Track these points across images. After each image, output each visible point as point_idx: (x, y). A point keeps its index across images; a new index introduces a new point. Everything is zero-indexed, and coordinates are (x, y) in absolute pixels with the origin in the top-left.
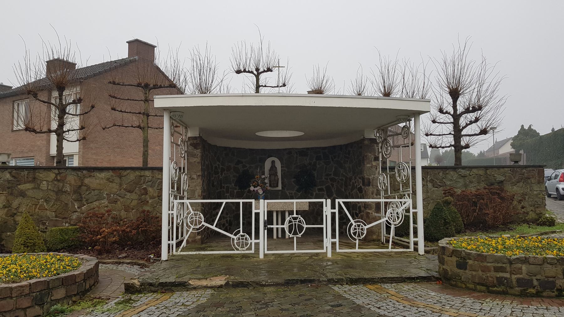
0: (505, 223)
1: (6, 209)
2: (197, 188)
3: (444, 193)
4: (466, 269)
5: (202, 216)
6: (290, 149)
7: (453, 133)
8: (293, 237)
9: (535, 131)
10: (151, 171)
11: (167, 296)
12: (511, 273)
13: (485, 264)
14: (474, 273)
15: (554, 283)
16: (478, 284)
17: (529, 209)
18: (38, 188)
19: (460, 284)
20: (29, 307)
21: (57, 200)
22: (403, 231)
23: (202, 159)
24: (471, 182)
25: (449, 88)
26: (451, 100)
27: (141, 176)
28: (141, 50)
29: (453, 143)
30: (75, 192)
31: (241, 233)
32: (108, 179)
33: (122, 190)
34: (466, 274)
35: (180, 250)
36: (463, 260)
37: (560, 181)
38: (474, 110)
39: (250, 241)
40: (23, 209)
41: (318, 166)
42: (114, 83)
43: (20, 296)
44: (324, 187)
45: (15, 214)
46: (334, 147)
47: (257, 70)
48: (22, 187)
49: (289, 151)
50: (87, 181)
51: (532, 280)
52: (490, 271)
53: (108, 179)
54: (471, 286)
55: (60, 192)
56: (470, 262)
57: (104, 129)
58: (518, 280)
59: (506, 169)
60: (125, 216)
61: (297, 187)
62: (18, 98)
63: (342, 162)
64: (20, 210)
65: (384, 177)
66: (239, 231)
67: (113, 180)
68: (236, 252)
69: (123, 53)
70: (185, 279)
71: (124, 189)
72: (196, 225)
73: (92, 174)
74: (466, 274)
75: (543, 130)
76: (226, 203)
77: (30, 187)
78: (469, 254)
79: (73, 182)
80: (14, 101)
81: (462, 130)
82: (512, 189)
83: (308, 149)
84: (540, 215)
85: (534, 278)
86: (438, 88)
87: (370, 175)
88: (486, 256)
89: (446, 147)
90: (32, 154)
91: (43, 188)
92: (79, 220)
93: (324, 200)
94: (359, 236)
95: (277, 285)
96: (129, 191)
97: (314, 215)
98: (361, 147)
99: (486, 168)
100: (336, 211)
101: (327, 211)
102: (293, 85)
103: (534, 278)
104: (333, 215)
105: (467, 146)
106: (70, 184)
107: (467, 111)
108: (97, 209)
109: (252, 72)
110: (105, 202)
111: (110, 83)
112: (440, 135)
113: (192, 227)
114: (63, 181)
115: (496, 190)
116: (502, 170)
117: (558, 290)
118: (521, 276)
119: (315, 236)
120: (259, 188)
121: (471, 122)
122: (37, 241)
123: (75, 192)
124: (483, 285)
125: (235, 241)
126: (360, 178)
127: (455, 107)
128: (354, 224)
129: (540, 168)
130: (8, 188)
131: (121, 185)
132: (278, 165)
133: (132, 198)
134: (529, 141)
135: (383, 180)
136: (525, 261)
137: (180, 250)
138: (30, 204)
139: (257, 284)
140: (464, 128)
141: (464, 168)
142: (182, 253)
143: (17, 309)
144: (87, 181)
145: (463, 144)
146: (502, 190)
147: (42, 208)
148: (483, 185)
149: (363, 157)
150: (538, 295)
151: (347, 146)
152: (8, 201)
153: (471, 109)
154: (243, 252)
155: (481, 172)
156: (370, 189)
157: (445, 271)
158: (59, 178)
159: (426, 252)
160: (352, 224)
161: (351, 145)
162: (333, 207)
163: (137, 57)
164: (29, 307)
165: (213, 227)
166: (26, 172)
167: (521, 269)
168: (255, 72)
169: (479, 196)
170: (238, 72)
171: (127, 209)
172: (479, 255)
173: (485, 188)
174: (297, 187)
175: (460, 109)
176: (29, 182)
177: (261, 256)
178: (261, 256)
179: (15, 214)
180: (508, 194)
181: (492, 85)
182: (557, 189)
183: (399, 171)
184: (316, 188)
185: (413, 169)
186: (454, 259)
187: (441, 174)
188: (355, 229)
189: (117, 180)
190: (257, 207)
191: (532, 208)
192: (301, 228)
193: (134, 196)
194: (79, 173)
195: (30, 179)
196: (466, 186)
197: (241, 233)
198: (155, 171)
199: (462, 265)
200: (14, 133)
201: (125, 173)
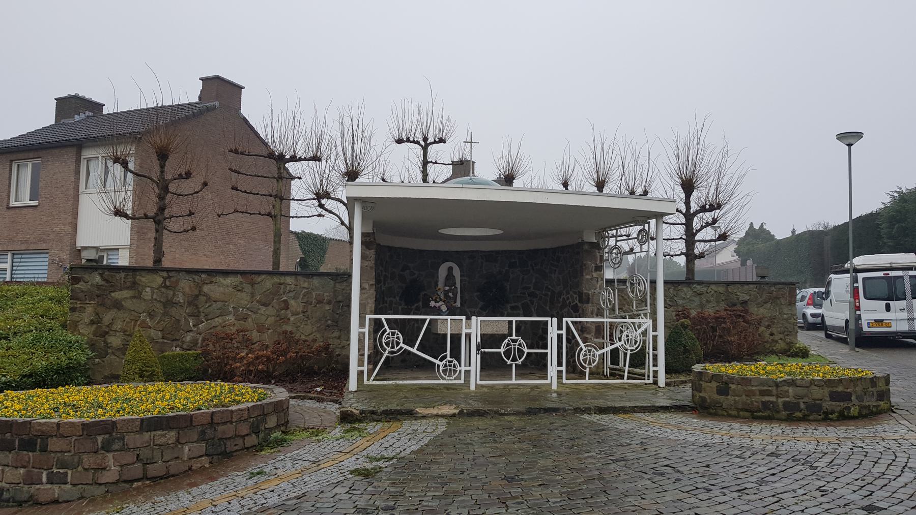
0: (751, 354)
1: (95, 326)
2: (369, 301)
3: (677, 315)
4: (728, 395)
5: (400, 335)
6: (473, 251)
7: (684, 237)
8: (511, 365)
9: (769, 233)
10: (293, 277)
11: (395, 424)
12: (778, 397)
13: (750, 388)
14: (737, 398)
15: (820, 406)
16: (742, 410)
17: (777, 337)
18: (138, 296)
19: (720, 412)
20: (247, 435)
21: (165, 314)
22: (638, 359)
23: (376, 264)
24: (708, 302)
25: (681, 178)
26: (683, 196)
27: (280, 284)
28: (221, 92)
29: (684, 251)
30: (190, 304)
31: (449, 358)
32: (235, 287)
33: (255, 302)
34: (727, 401)
35: (372, 378)
36: (724, 385)
37: (808, 304)
38: (712, 208)
39: (458, 369)
40: (118, 326)
41: (511, 276)
42: (236, 152)
43: (239, 421)
44: (519, 304)
45: (107, 333)
46: (536, 251)
47: (425, 139)
48: (116, 295)
49: (472, 255)
50: (206, 289)
51: (799, 403)
52: (754, 395)
53: (235, 287)
54: (734, 413)
55: (169, 303)
56: (733, 387)
57: (219, 216)
58: (785, 403)
59: (752, 286)
60: (258, 339)
61: (481, 304)
62: (21, 156)
63: (547, 271)
64: (114, 327)
65: (610, 293)
66: (445, 357)
67: (243, 288)
68: (442, 382)
69: (191, 94)
70: (408, 406)
71: (258, 301)
72: (393, 347)
73: (214, 280)
74: (727, 401)
75: (781, 232)
76: (431, 320)
77: (128, 296)
78: (733, 378)
79: (187, 290)
80: (11, 161)
81: (696, 234)
82: (757, 311)
83: (498, 252)
84: (790, 344)
85: (801, 401)
86: (669, 181)
87: (590, 290)
88: (750, 380)
89: (305, 159)
90: (44, 246)
91: (146, 298)
92: (194, 343)
93: (549, 319)
94: (590, 364)
95: (517, 413)
96: (265, 305)
97: (537, 336)
98: (578, 253)
99: (728, 284)
100: (564, 332)
101: (553, 332)
102: (538, 183)
103: (801, 401)
104: (560, 337)
105: (702, 256)
106: (184, 293)
107: (703, 209)
108: (219, 328)
109: (418, 143)
110: (231, 318)
111: (231, 151)
112: (668, 239)
113: (388, 349)
114: (173, 287)
115: (739, 312)
116: (746, 287)
117: (824, 413)
118: (787, 399)
119: (537, 365)
120: (441, 303)
121: (707, 225)
122: (155, 368)
123: (190, 304)
124: (746, 410)
125: (441, 369)
126: (575, 293)
127: (687, 203)
128: (584, 349)
129: (792, 287)
130: (98, 296)
131: (253, 295)
132: (457, 272)
133: (267, 315)
134: (760, 246)
135: (608, 296)
136: (792, 383)
137: (372, 378)
138: (127, 320)
139: (495, 413)
140: (698, 231)
141: (700, 283)
142: (375, 382)
143: (237, 436)
144: (206, 289)
145: (696, 252)
146: (746, 312)
147: (144, 326)
148: (723, 305)
149: (581, 267)
150: (804, 419)
151: (554, 250)
152: (97, 314)
153: (707, 207)
154: (450, 382)
155: (721, 289)
156: (590, 307)
157: (703, 399)
158: (168, 283)
159: (667, 384)
160: (581, 349)
161: (562, 249)
162: (560, 327)
163: (217, 103)
164: (247, 435)
165: (414, 350)
166: (123, 275)
167: (787, 392)
168: (423, 143)
169: (718, 319)
170: (400, 141)
171: (261, 329)
172: (743, 378)
173: (726, 310)
174: (481, 304)
175: (694, 207)
176: (128, 288)
177: (473, 387)
178: (473, 387)
179: (107, 333)
180: (754, 317)
181: (736, 177)
182: (804, 315)
183: (632, 284)
184: (509, 306)
185: (653, 283)
186: (714, 384)
187: (671, 290)
188: (585, 355)
189: (248, 288)
190: (469, 326)
191: (781, 336)
192: (521, 353)
193: (270, 311)
194: (196, 277)
195: (128, 284)
196: (702, 306)
197: (449, 358)
198: (299, 277)
199: (724, 390)
200: (12, 212)
201: (259, 279)
